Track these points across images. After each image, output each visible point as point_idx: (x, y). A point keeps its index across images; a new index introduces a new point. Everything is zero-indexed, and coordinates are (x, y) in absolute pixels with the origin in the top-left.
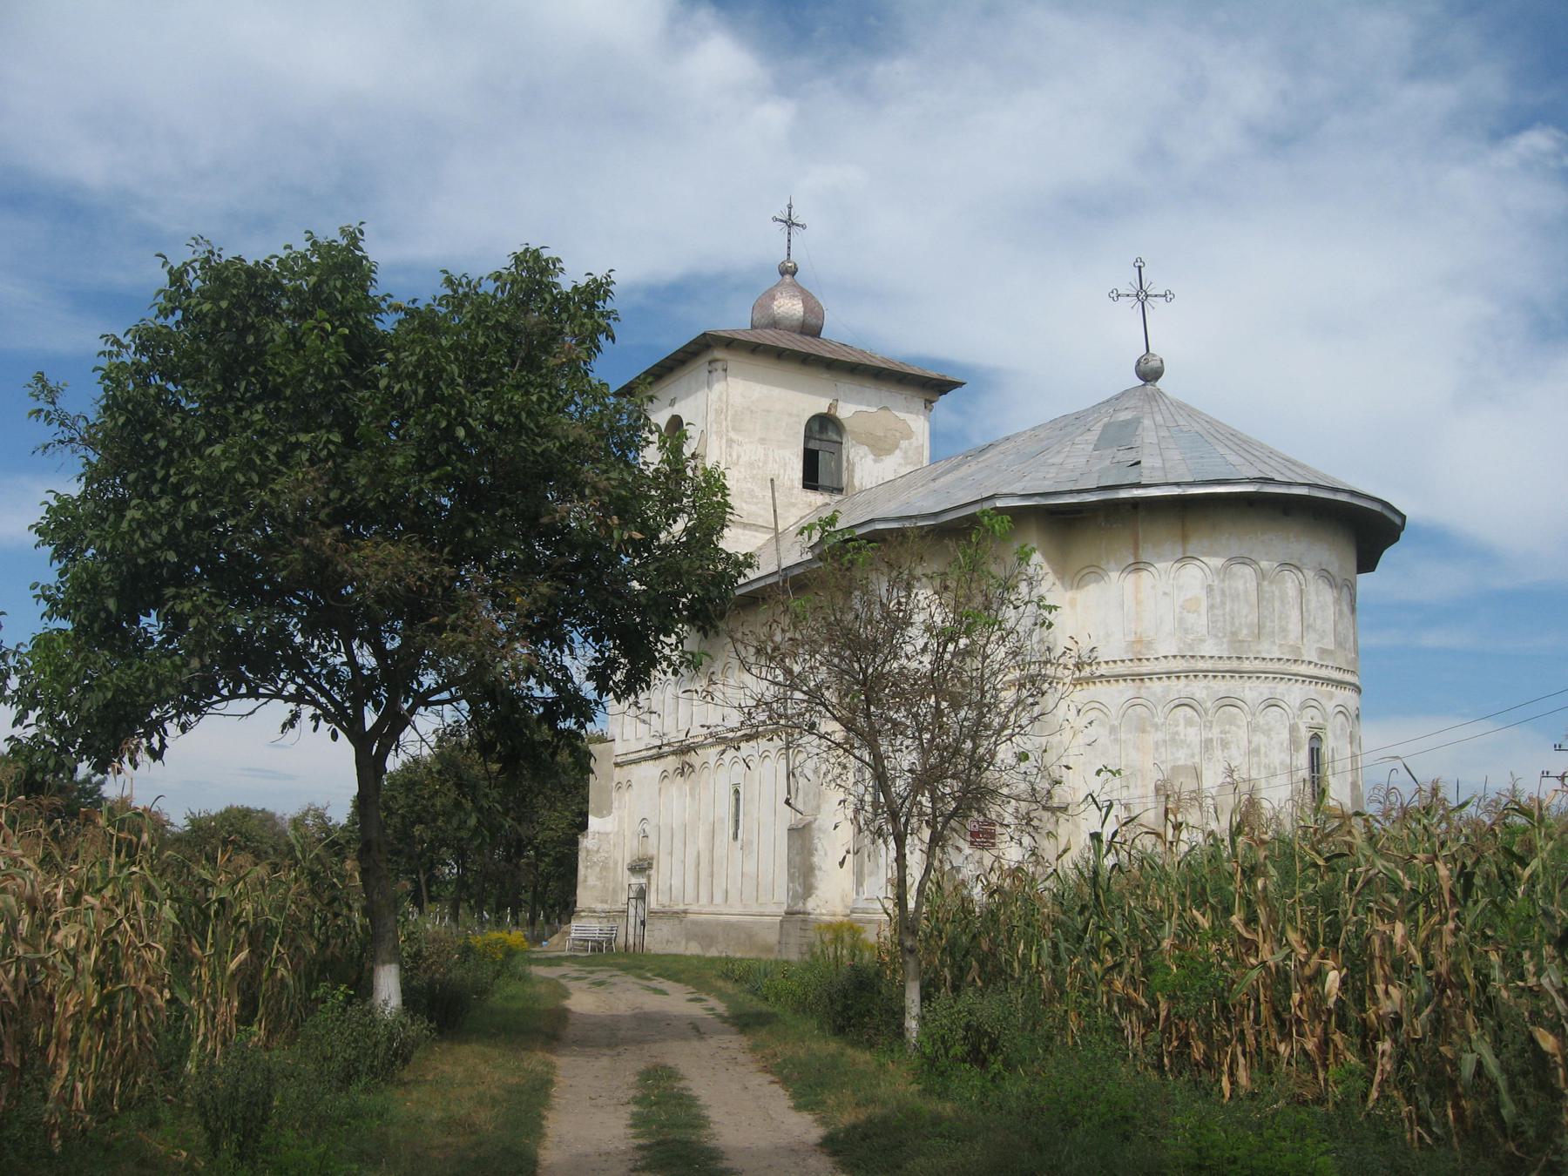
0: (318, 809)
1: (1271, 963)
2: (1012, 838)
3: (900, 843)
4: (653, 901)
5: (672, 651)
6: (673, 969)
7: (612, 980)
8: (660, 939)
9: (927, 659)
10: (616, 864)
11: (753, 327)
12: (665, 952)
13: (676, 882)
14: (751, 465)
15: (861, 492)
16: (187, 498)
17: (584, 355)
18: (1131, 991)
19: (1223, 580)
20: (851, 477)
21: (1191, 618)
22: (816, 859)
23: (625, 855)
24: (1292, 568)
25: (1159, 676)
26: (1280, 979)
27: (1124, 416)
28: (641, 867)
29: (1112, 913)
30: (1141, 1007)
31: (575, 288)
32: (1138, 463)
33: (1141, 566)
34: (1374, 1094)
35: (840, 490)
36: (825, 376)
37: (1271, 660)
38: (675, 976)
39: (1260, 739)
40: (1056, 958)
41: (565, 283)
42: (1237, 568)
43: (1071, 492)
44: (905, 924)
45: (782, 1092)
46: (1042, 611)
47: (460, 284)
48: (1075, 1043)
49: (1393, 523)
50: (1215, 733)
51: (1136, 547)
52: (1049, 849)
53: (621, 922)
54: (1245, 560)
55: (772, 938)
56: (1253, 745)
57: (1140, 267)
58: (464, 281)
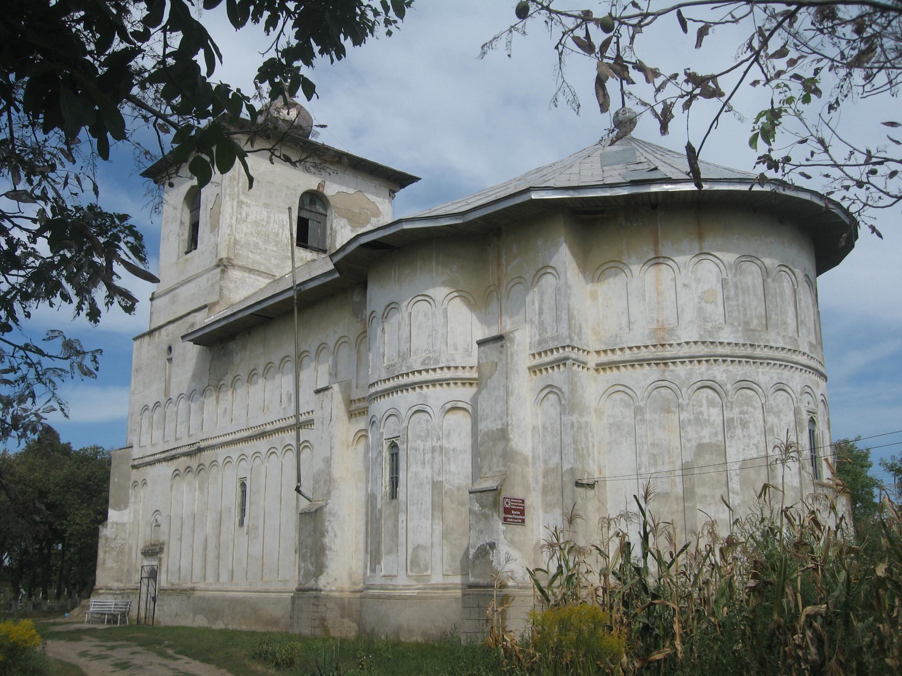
4: (163, 580)
7: (138, 660)
10: (131, 549)
12: (175, 624)
13: (185, 564)
14: (256, 223)
19: (735, 276)
21: (709, 308)
22: (327, 540)
23: (139, 541)
24: (787, 270)
25: (683, 360)
28: (153, 551)
33: (661, 260)
37: (777, 348)
42: (745, 265)
50: (734, 413)
51: (656, 243)
54: (752, 258)
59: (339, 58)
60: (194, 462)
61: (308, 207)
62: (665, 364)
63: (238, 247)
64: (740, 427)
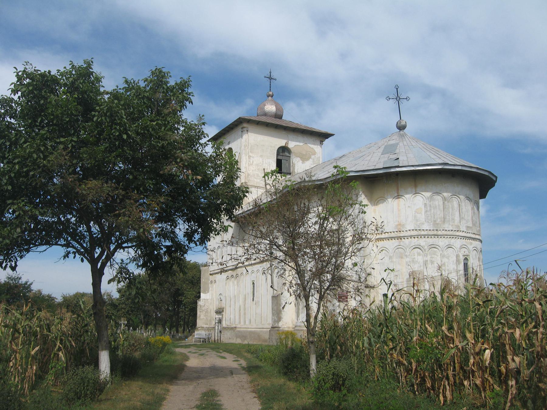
0: (108, 293)
1: (460, 347)
2: (352, 297)
3: (307, 300)
4: (224, 324)
5: (216, 225)
6: (230, 349)
8: (227, 338)
9: (317, 227)
11: (258, 116)
12: (229, 342)
13: (232, 317)
14: (257, 165)
15: (297, 174)
16: (15, 164)
17: (179, 108)
18: (400, 358)
20: (294, 169)
26: (464, 352)
27: (392, 142)
28: (220, 311)
29: (392, 326)
30: (404, 365)
31: (176, 83)
32: (398, 159)
33: (400, 197)
34: (508, 404)
35: (290, 174)
36: (284, 133)
37: (449, 230)
38: (230, 352)
39: (445, 260)
40: (370, 344)
41: (172, 82)
43: (373, 170)
44: (310, 331)
45: (258, 402)
46: (361, 207)
47: (131, 82)
48: (378, 380)
49: (492, 179)
50: (428, 258)
51: (398, 190)
52: (367, 302)
53: (213, 332)
54: (438, 193)
55: (267, 336)
56: (443, 262)
57: (397, 88)
58: (132, 81)
59: (209, 241)
60: (234, 273)
61: (281, 154)
62: (401, 239)
63: (249, 177)
64: (430, 263)
